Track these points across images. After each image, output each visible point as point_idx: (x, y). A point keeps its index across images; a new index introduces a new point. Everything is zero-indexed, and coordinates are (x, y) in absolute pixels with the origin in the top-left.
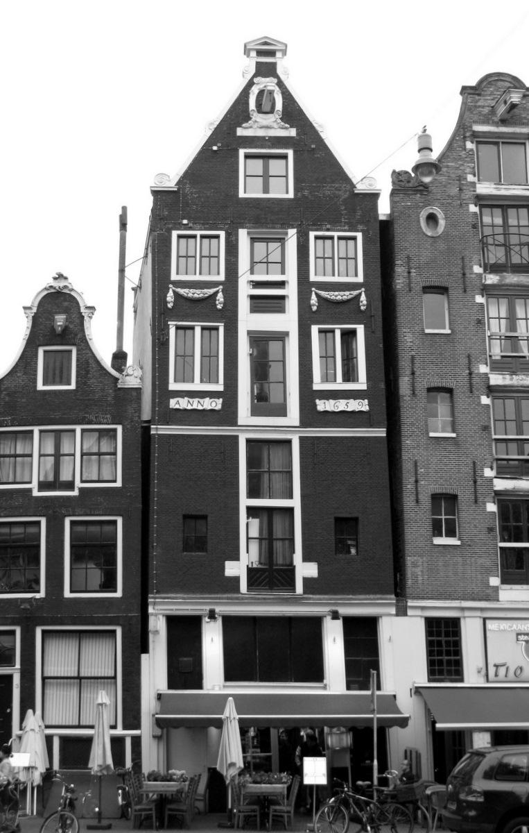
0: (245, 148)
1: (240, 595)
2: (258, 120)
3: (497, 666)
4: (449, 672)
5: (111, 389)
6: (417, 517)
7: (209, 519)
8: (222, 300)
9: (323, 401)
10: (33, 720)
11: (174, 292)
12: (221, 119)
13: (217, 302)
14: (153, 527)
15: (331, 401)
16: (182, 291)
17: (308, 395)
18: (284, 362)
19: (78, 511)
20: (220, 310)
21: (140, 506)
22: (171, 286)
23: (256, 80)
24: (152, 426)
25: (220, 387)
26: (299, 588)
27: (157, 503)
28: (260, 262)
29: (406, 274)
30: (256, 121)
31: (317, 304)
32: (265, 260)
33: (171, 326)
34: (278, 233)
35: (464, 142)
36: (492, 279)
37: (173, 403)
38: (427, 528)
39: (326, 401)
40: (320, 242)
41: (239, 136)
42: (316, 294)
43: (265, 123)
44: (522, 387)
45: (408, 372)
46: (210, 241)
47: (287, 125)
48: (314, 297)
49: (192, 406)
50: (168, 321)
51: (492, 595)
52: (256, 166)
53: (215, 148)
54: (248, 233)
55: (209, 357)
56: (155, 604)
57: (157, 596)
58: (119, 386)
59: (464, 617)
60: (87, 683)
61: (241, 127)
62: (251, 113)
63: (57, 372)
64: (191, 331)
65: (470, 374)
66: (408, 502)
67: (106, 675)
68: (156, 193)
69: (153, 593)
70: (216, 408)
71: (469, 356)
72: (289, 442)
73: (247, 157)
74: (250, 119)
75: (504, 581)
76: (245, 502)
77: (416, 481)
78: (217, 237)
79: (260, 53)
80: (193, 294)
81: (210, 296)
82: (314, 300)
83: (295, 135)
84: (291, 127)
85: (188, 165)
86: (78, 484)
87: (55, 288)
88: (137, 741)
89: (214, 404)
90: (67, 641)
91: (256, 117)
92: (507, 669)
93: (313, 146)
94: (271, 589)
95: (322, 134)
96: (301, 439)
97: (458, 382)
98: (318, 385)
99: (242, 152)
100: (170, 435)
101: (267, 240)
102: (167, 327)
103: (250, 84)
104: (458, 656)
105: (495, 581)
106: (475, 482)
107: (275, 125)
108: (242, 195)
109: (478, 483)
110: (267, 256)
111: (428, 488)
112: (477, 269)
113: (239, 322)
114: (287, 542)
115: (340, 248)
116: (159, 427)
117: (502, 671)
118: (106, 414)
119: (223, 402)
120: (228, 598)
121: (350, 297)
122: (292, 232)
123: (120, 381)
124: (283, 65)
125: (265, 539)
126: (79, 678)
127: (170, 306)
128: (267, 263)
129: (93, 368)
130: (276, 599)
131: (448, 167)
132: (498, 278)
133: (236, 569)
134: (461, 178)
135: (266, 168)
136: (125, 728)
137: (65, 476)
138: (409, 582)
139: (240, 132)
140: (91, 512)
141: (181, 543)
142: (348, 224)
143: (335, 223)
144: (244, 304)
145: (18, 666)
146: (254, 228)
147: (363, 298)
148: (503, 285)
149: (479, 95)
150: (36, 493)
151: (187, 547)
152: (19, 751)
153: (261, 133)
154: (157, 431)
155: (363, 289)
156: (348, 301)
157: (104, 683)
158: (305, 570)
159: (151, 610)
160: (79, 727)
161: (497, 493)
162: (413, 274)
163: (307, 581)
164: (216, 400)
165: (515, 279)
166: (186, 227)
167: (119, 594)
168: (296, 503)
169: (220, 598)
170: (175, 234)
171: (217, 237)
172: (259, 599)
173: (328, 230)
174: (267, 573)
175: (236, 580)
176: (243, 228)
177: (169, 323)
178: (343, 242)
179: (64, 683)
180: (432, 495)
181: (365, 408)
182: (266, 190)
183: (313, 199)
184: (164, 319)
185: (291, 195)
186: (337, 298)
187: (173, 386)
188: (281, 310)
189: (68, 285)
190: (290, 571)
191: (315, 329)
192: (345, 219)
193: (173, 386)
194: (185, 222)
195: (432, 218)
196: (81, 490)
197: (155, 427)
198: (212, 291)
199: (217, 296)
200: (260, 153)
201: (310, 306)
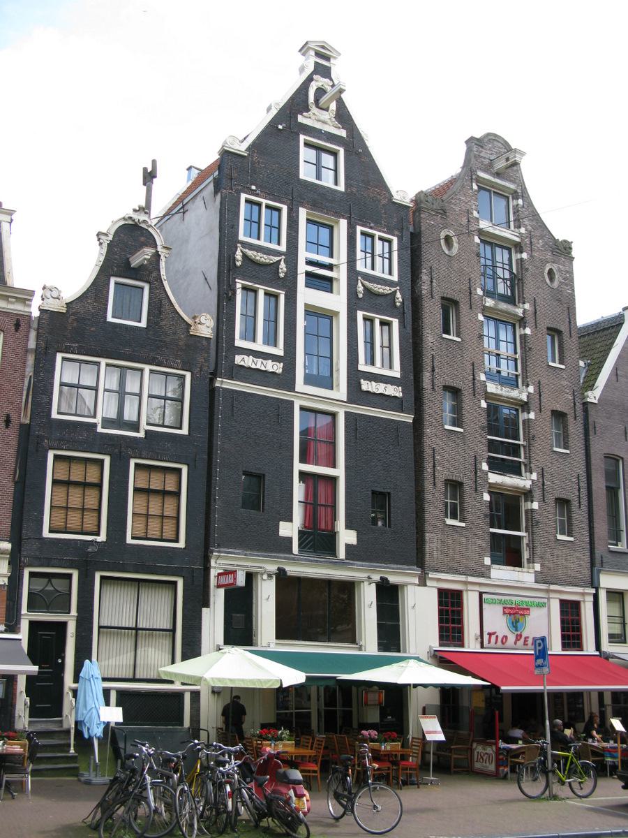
3: (490, 634)
4: (454, 638)
5: (183, 334)
6: (435, 497)
9: (367, 382)
10: (92, 668)
16: (250, 253)
17: (355, 376)
19: (145, 453)
22: (239, 245)
24: (218, 379)
25: (279, 351)
26: (342, 554)
29: (429, 283)
35: (472, 182)
36: (489, 302)
37: (239, 359)
38: (440, 510)
42: (363, 285)
43: (322, 118)
44: (507, 397)
45: (429, 369)
48: (360, 284)
50: (235, 278)
51: (485, 573)
53: (280, 127)
55: (272, 321)
56: (218, 557)
58: (191, 333)
59: (467, 591)
60: (110, 633)
63: (128, 307)
65: (474, 379)
66: (428, 483)
67: (161, 627)
70: (277, 372)
71: (473, 364)
75: (493, 562)
76: (298, 466)
77: (434, 466)
79: (318, 54)
82: (360, 288)
84: (342, 128)
86: (144, 426)
87: (134, 220)
89: (275, 367)
90: (147, 590)
91: (314, 109)
92: (497, 637)
93: (360, 151)
94: (315, 552)
96: (347, 414)
97: (465, 386)
100: (233, 390)
103: (310, 79)
104: (460, 624)
105: (487, 561)
106: (476, 473)
109: (478, 475)
111: (443, 474)
112: (480, 292)
113: (298, 294)
114: (329, 509)
116: (225, 380)
117: (493, 638)
120: (285, 558)
121: (390, 292)
122: (343, 223)
123: (192, 328)
124: (338, 69)
125: (310, 504)
126: (137, 629)
130: (326, 562)
131: (460, 199)
132: (493, 302)
133: (289, 530)
134: (469, 212)
137: (130, 414)
138: (427, 555)
140: (158, 457)
141: (240, 499)
143: (378, 225)
144: (301, 279)
145: (74, 612)
146: (312, 210)
147: (398, 295)
148: (496, 310)
149: (482, 147)
150: (100, 430)
151: (244, 506)
152: (436, 705)
153: (318, 126)
155: (398, 288)
156: (387, 295)
157: (107, 633)
158: (346, 537)
160: (134, 680)
161: (491, 485)
162: (434, 284)
163: (348, 547)
164: (278, 364)
165: (505, 307)
166: (254, 193)
168: (339, 472)
169: (278, 558)
172: (312, 561)
173: (371, 228)
175: (290, 540)
179: (107, 633)
180: (445, 480)
181: (399, 395)
183: (359, 197)
187: (239, 343)
189: (148, 220)
191: (360, 315)
194: (254, 187)
195: (448, 240)
196: (147, 432)
197: (220, 379)
198: (277, 259)
201: (356, 293)
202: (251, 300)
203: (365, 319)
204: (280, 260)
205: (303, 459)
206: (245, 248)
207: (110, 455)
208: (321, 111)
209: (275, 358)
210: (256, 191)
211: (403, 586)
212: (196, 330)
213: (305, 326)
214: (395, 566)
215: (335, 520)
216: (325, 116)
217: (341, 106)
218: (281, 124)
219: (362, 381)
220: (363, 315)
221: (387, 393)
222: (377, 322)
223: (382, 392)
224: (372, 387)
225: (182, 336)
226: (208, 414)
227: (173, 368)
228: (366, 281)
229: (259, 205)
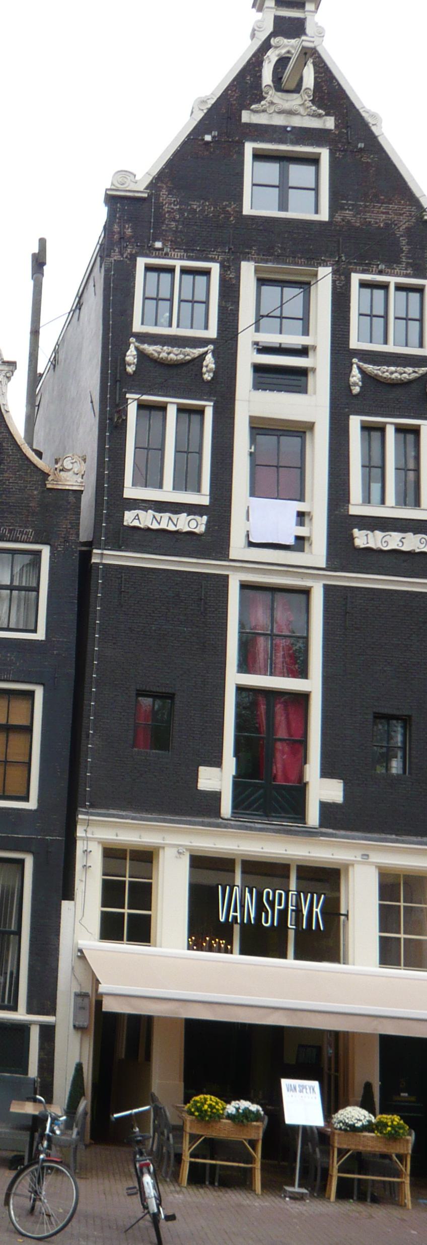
0: (254, 140)
1: (220, 820)
2: (275, 101)
7: (177, 700)
8: (213, 366)
9: (364, 532)
11: (137, 349)
12: (218, 96)
13: (204, 370)
14: (90, 705)
15: (377, 532)
16: (150, 349)
18: (302, 469)
20: (208, 382)
21: (72, 671)
22: (132, 340)
23: (273, 41)
24: (95, 551)
25: (203, 499)
26: (313, 816)
27: (97, 669)
28: (267, 316)
30: (272, 103)
31: (360, 383)
32: (277, 313)
33: (129, 401)
34: (300, 273)
37: (130, 518)
39: (369, 532)
40: (153, 276)
41: (245, 124)
42: (359, 368)
43: (287, 106)
46: (159, 276)
47: (321, 111)
48: (355, 371)
49: (159, 523)
50: (126, 393)
52: (271, 171)
53: (208, 138)
54: (257, 270)
56: (88, 823)
57: (91, 810)
58: (49, 486)
61: (249, 109)
62: (265, 90)
64: (160, 413)
68: (112, 200)
69: (85, 806)
70: (196, 531)
72: (306, 592)
73: (259, 156)
74: (265, 98)
78: (207, 273)
80: (169, 353)
81: (194, 360)
82: (355, 376)
83: (332, 127)
84: (327, 114)
85: (165, 162)
88: (48, 1033)
91: (272, 96)
93: (361, 145)
94: (267, 816)
95: (374, 129)
96: (327, 588)
98: (357, 507)
99: (249, 148)
101: (283, 283)
102: (125, 401)
103: (266, 46)
107: (301, 110)
108: (247, 210)
110: (281, 306)
115: (182, 285)
116: (106, 552)
118: (26, 527)
119: (208, 522)
121: (414, 376)
122: (325, 273)
123: (50, 478)
127: (130, 369)
128: (281, 317)
129: (9, 456)
135: (284, 175)
136: (30, 1011)
139: (246, 117)
142: (412, 267)
143: (391, 262)
144: (244, 377)
154: (102, 559)
156: (410, 382)
159: (80, 832)
163: (326, 808)
167: (32, 804)
168: (234, 678)
170: (141, 262)
171: (207, 273)
173: (380, 273)
174: (261, 791)
175: (216, 797)
176: (248, 260)
177: (128, 396)
178: (188, 278)
182: (283, 206)
184: (121, 389)
185: (324, 215)
186: (393, 376)
187: (130, 492)
188: (302, 389)
190: (300, 790)
191: (355, 422)
192: (408, 258)
193: (130, 492)
194: (158, 245)
197: (99, 551)
198: (197, 352)
199: (204, 359)
200: (293, 151)
201: (348, 387)
202: (376, 445)
203: (366, 428)
204: (206, 353)
205: (245, 666)
206: (143, 343)
207: (43, 684)
208: (284, 95)
209: (193, 510)
210: (162, 249)
211: (347, 866)
212: (56, 480)
213: (251, 454)
214: (414, 839)
215: (305, 763)
216: (294, 101)
217: (324, 74)
218: (209, 133)
219: (356, 532)
220: (362, 422)
221: (404, 549)
222: (390, 432)
223: (395, 547)
224: (375, 540)
225: (35, 492)
226: (76, 606)
227: (21, 542)
228: (369, 363)
229: (385, 287)
